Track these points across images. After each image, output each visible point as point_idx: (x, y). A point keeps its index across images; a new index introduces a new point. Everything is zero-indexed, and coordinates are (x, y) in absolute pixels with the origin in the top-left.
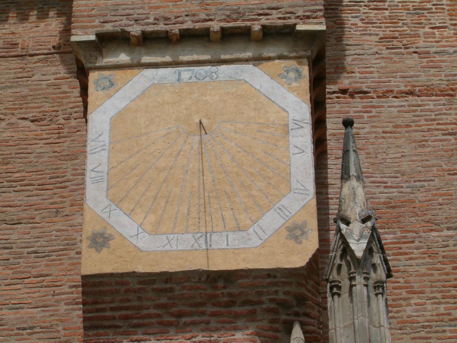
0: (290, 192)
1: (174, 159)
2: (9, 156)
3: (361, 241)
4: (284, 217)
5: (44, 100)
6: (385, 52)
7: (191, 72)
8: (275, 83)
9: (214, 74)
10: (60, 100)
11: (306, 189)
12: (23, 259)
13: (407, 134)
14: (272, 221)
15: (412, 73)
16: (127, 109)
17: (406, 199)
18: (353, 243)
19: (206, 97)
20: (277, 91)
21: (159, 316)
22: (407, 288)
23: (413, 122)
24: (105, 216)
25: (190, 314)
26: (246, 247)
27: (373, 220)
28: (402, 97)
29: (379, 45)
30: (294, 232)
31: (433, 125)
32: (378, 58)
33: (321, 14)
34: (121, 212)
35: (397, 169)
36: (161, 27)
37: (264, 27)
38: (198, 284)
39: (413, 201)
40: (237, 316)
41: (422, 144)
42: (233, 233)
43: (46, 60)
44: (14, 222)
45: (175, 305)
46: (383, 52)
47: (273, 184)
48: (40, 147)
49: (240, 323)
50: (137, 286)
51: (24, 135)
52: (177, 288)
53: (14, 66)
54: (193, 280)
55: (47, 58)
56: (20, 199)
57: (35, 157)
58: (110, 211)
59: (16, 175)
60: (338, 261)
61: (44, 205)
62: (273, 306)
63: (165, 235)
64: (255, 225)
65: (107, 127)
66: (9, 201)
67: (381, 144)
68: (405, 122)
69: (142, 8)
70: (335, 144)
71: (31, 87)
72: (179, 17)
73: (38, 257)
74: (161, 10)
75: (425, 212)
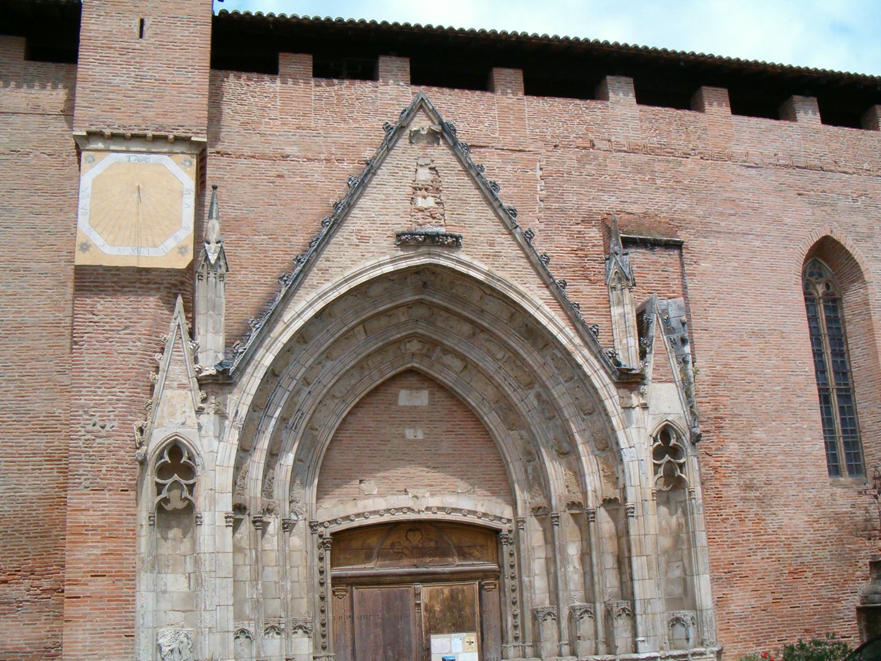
14: (171, 244)
20: (179, 171)
24: (87, 234)
36: (121, 131)
39: (247, 218)
40: (152, 289)
41: (255, 186)
43: (55, 119)
48: (52, 171)
49: (152, 293)
60: (203, 263)
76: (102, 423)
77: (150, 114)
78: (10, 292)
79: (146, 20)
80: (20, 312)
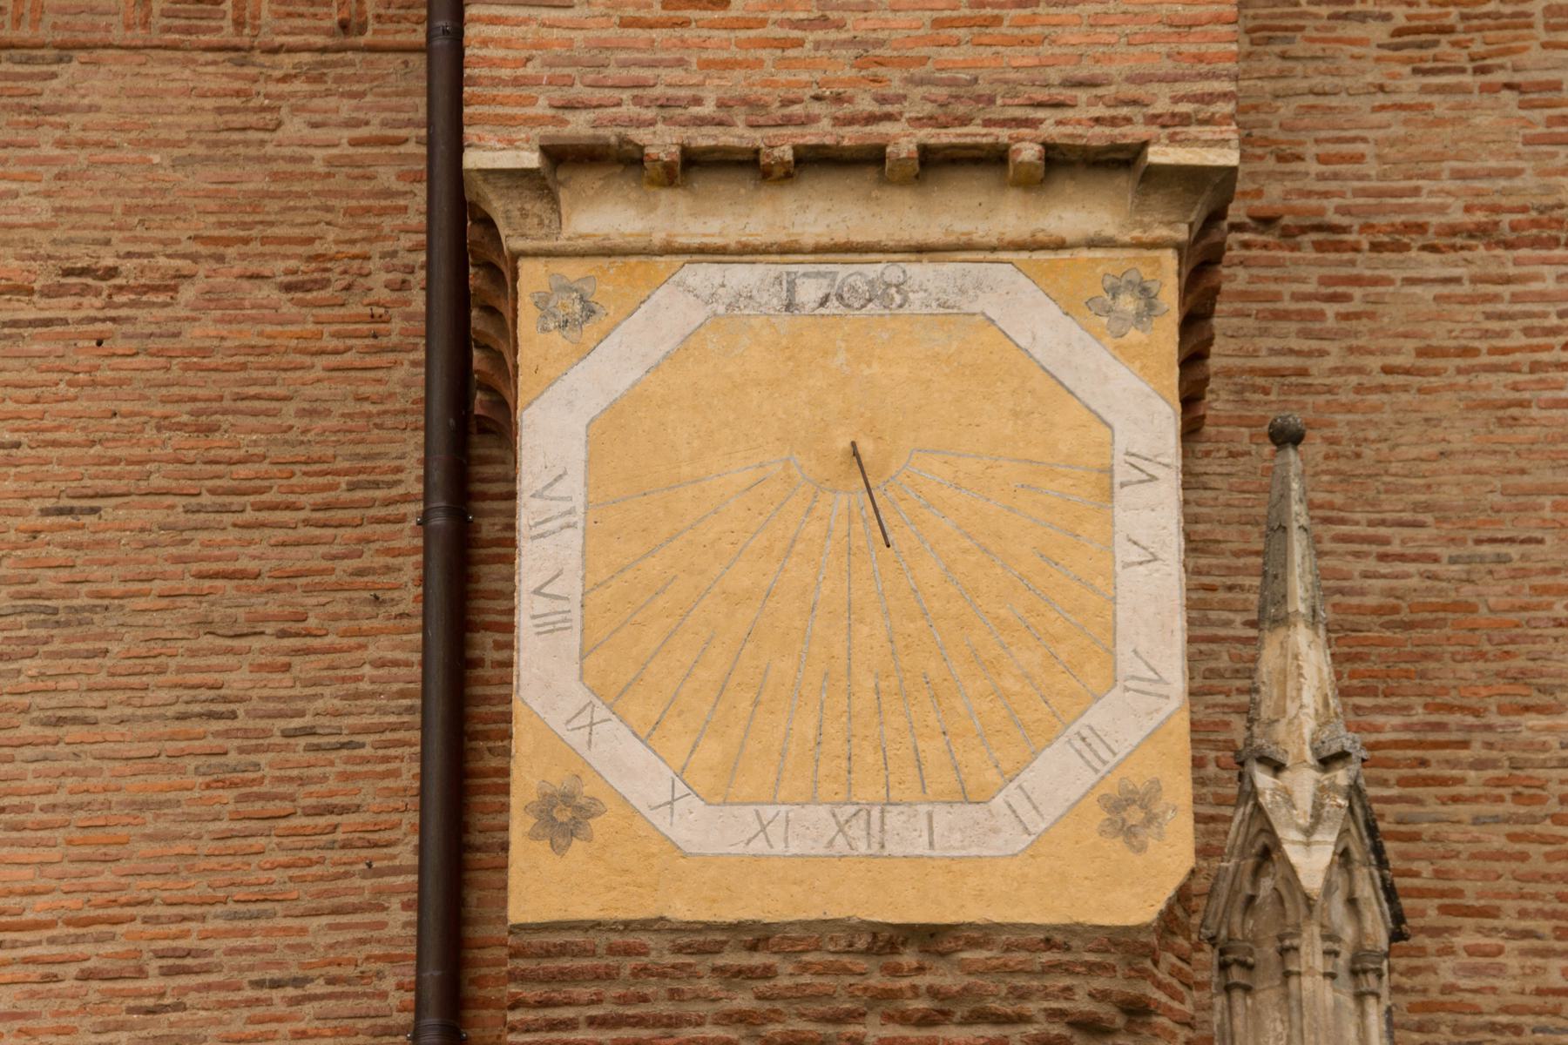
0: (1114, 686)
1: (777, 567)
2: (215, 405)
3: (1317, 837)
4: (1096, 763)
5: (320, 215)
6: (1409, 87)
7: (825, 282)
8: (1075, 328)
9: (893, 290)
10: (373, 220)
11: (1161, 680)
12: (270, 755)
13: (1462, 380)
14: (1060, 778)
15: (1492, 163)
17: (1449, 600)
18: (1293, 842)
19: (869, 365)
22: (1442, 894)
23: (1486, 334)
24: (576, 739)
26: (985, 853)
27: (1355, 767)
28: (1453, 248)
29: (1390, 59)
30: (1124, 815)
31: (1550, 348)
32: (1382, 108)
33: (1227, 108)
34: (622, 727)
35: (1423, 498)
36: (738, 136)
38: (846, 959)
39: (1470, 608)
41: (1508, 412)
42: (947, 808)
44: (237, 630)
46: (1402, 83)
47: (1063, 657)
50: (670, 959)
51: (261, 334)
53: (213, 86)
54: (831, 948)
55: (323, 64)
56: (255, 553)
57: (302, 413)
58: (592, 724)
59: (243, 471)
61: (333, 578)
63: (753, 808)
64: (1012, 786)
65: (578, 453)
66: (218, 559)
67: (1375, 409)
68: (1456, 338)
69: (680, 63)
70: (1229, 407)
71: (275, 167)
72: (793, 102)
73: (317, 748)
74: (738, 74)
75: (1506, 648)
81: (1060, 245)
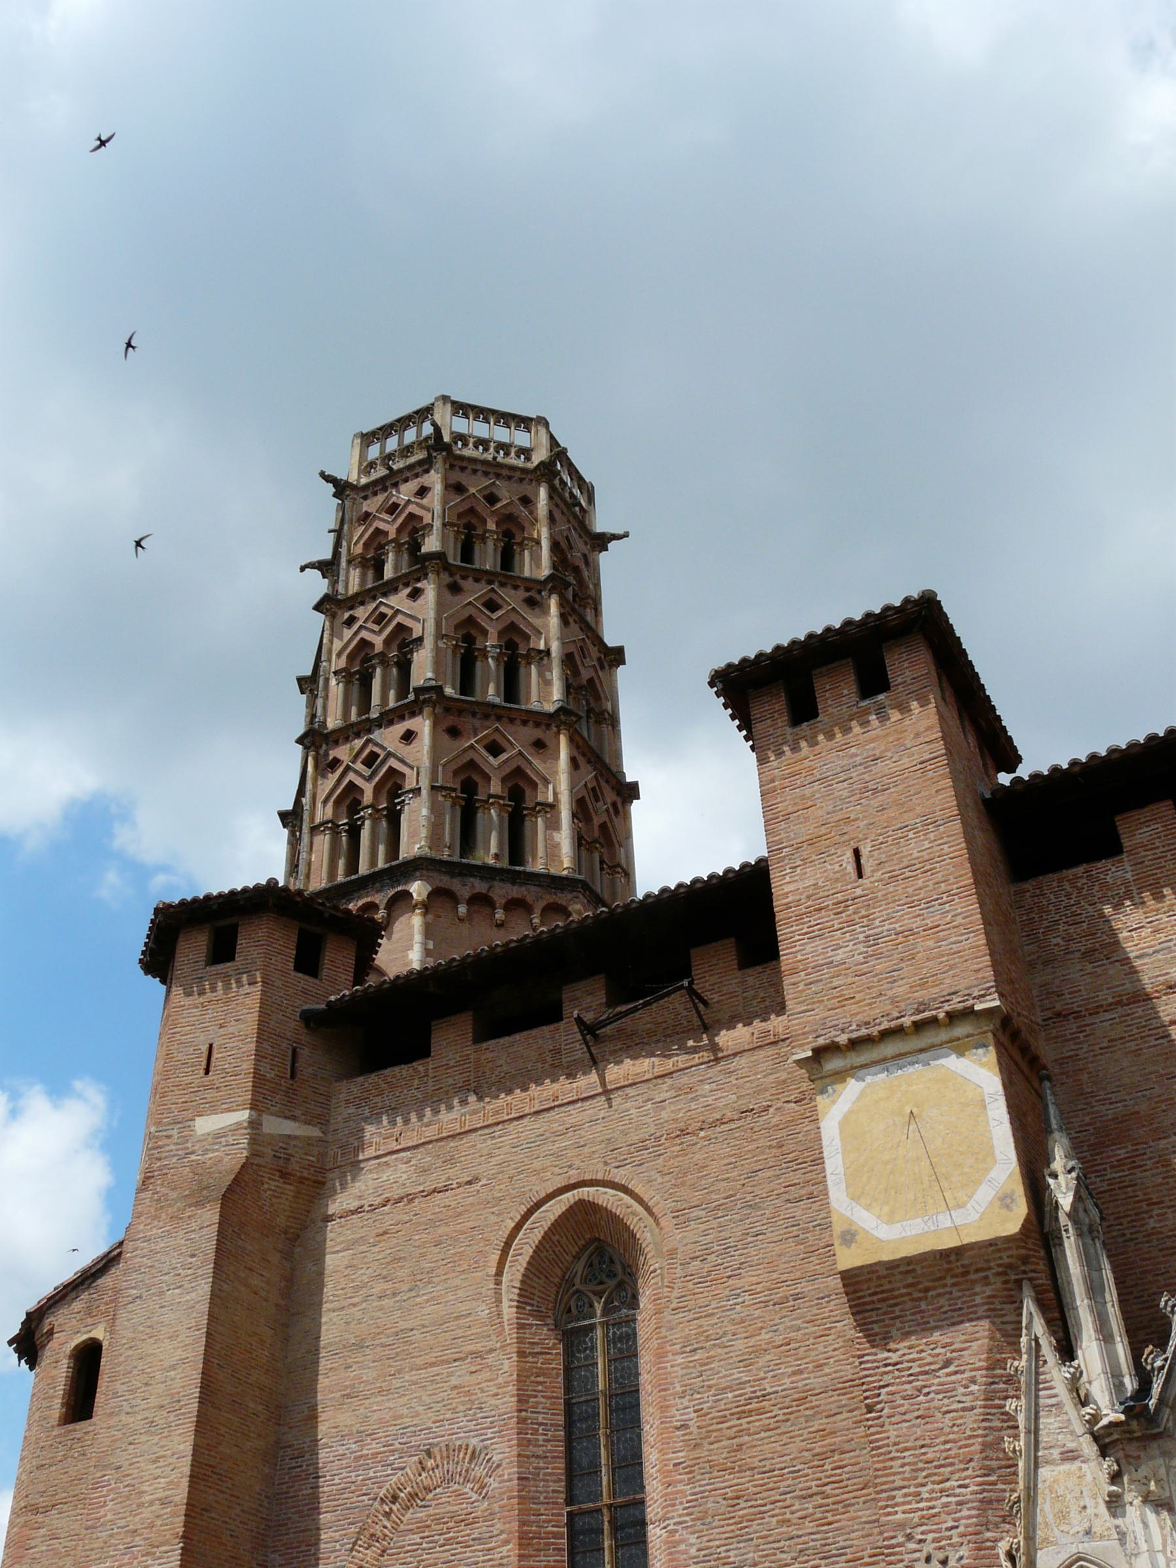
6: (1089, 968)
14: (985, 1194)
16: (850, 1112)
21: (909, 1294)
24: (848, 1214)
25: (935, 1288)
33: (994, 990)
36: (864, 1032)
37: (947, 1013)
39: (1138, 1113)
41: (1137, 1052)
45: (921, 1282)
50: (885, 1272)
52: (918, 1268)
62: (1000, 1270)
76: (941, 1555)
77: (900, 989)
78: (779, 1340)
79: (202, 1072)
80: (801, 1372)
81: (959, 1039)
